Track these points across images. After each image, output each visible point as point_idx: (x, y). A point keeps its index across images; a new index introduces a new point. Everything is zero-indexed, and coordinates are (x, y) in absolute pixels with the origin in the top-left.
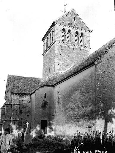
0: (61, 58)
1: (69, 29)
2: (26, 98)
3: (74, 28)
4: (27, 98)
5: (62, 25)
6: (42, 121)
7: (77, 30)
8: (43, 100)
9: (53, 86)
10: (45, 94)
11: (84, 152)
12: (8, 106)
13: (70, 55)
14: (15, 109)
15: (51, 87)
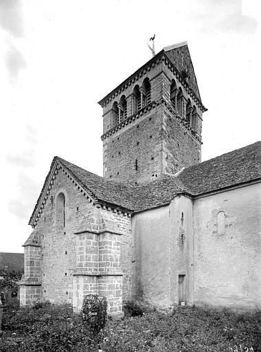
12: (91, 238)
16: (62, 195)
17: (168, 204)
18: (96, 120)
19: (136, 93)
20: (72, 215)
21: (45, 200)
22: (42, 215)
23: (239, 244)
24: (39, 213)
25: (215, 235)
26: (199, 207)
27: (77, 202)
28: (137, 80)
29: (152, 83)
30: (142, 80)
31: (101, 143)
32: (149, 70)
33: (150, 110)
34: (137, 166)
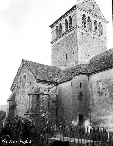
0: (82, 46)
1: (88, 15)
2: (52, 87)
3: (93, 16)
4: (54, 88)
5: (83, 10)
6: (79, 115)
7: (95, 19)
8: (79, 91)
9: (89, 75)
10: (81, 83)
11: (11, 142)
12: (34, 97)
13: (90, 44)
14: (44, 100)
15: (85, 76)
16: (25, 76)
17: (71, 80)
18: (49, 34)
19: (70, 20)
20: (28, 86)
21: (18, 78)
22: (16, 85)
23: (109, 98)
24: (15, 84)
25: (99, 93)
26: (91, 79)
27: (31, 80)
28: (66, 16)
29: (72, 18)
30: (59, 24)
31: (51, 45)
32: (71, 13)
33: (72, 30)
34: (67, 57)
